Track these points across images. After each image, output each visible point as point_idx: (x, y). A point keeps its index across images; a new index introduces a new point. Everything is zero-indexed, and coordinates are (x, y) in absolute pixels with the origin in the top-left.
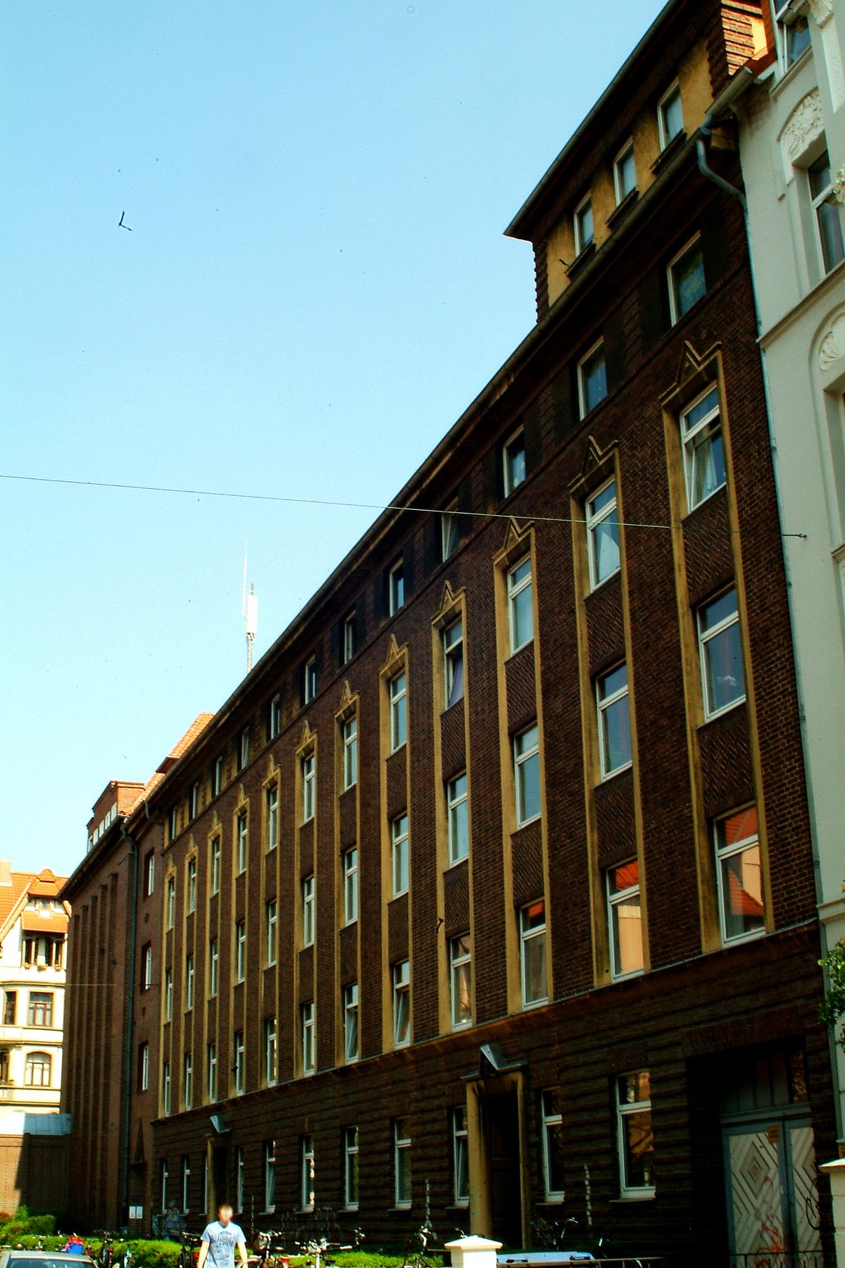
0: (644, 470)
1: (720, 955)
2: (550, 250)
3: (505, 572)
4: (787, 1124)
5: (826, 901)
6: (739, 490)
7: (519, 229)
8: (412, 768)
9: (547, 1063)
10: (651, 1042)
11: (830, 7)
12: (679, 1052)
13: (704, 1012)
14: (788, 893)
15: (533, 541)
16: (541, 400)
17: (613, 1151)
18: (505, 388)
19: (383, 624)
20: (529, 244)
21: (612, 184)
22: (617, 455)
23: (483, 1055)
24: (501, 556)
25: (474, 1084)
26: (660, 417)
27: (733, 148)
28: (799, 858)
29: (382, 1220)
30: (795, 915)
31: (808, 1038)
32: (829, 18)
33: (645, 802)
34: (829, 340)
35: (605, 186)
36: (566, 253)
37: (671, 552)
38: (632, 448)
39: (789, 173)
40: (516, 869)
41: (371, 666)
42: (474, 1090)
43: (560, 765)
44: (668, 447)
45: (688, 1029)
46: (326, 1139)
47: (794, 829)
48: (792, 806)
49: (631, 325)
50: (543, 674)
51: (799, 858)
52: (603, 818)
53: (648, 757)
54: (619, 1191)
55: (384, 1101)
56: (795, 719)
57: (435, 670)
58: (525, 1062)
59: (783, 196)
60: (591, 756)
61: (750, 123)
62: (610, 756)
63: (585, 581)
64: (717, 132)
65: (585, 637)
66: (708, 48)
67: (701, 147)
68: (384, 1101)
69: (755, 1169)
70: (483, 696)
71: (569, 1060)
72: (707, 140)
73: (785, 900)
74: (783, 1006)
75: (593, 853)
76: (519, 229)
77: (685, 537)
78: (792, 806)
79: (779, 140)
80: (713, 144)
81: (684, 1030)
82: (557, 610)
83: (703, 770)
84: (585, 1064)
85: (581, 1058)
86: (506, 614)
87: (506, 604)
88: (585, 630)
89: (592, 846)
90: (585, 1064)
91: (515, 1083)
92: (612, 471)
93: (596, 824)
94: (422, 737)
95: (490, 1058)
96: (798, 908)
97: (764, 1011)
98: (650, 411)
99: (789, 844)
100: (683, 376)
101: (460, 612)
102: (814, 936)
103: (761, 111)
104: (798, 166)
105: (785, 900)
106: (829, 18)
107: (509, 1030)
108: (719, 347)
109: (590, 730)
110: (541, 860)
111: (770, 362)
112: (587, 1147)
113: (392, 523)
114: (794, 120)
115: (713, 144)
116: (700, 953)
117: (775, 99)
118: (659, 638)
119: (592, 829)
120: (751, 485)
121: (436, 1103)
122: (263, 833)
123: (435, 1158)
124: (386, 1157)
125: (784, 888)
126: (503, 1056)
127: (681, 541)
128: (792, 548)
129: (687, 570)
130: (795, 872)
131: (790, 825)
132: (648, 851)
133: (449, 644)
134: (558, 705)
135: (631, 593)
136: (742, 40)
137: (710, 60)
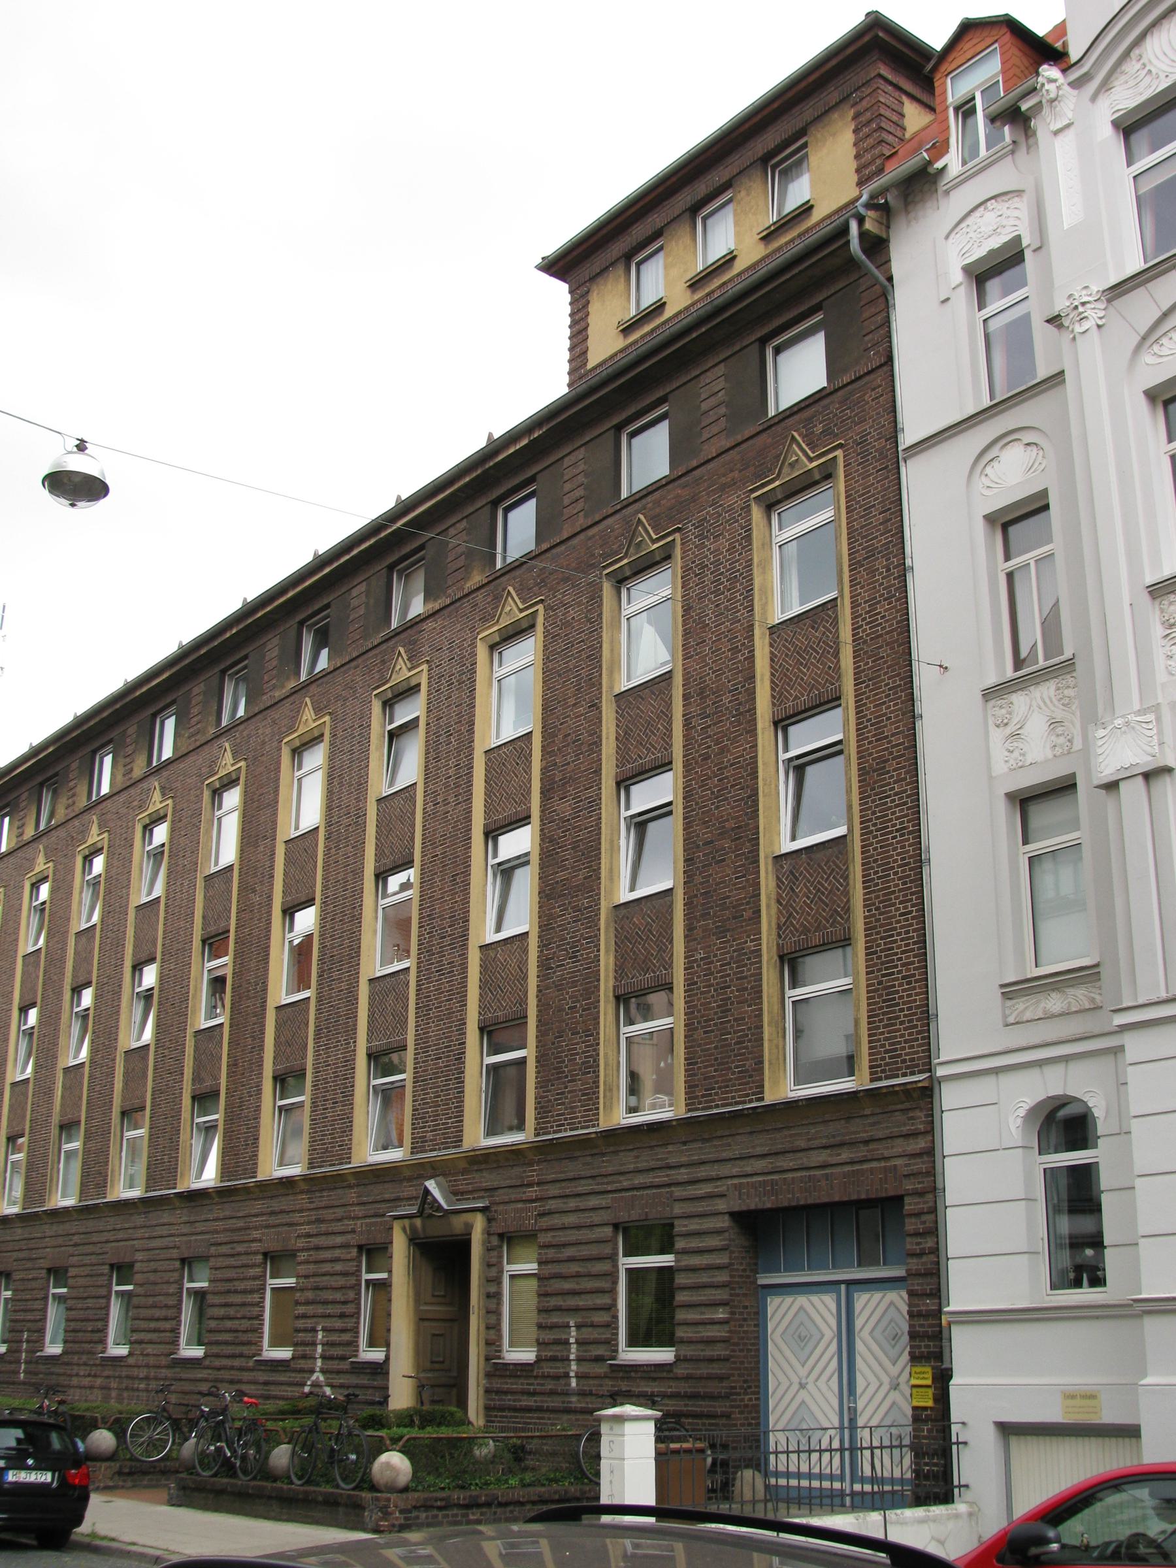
0: (717, 563)
1: (792, 1106)
2: (594, 297)
3: (492, 648)
4: (852, 1287)
5: (942, 1059)
6: (855, 605)
7: (560, 265)
8: (327, 853)
9: (520, 1205)
10: (678, 1192)
11: (1070, 115)
12: (721, 1205)
13: (760, 1165)
14: (890, 1045)
15: (540, 620)
16: (567, 462)
17: (611, 1308)
18: (525, 442)
19: (292, 684)
20: (564, 287)
21: (694, 240)
22: (678, 542)
23: (427, 1192)
24: (491, 631)
25: (407, 1222)
26: (747, 509)
27: (884, 236)
28: (909, 1009)
29: (241, 1369)
30: (898, 1069)
31: (907, 1200)
32: (1068, 126)
33: (689, 928)
34: (995, 463)
35: (687, 240)
36: (613, 308)
37: (751, 658)
38: (701, 536)
39: (958, 276)
40: (484, 985)
41: (268, 731)
42: (404, 1229)
43: (562, 875)
44: (756, 544)
45: (735, 1181)
46: (155, 1271)
47: (904, 978)
48: (903, 952)
49: (712, 401)
50: (544, 771)
51: (909, 1009)
52: (622, 942)
53: (698, 879)
54: (616, 1351)
55: (256, 1234)
56: (915, 864)
57: (372, 747)
58: (487, 1203)
59: (948, 299)
60: (611, 870)
61: (907, 212)
62: (642, 873)
63: (616, 675)
64: (871, 214)
65: (613, 737)
66: (854, 119)
67: (854, 226)
68: (256, 1234)
69: (802, 1338)
70: (447, 786)
71: (552, 1205)
72: (861, 220)
73: (886, 1052)
74: (874, 1164)
75: (607, 976)
76: (560, 265)
77: (771, 645)
78: (903, 952)
79: (947, 237)
80: (868, 225)
81: (730, 1182)
82: (571, 701)
83: (778, 902)
84: (577, 1210)
85: (572, 1204)
86: (489, 695)
87: (490, 685)
88: (613, 729)
89: (606, 970)
90: (577, 1210)
91: (469, 1228)
92: (668, 557)
93: (613, 947)
94: (346, 821)
95: (436, 1193)
96: (904, 1061)
97: (847, 1168)
98: (733, 499)
99: (897, 992)
100: (786, 470)
101: (419, 685)
102: (924, 1097)
103: (923, 200)
104: (967, 270)
105: (886, 1052)
106: (1068, 126)
107: (463, 1165)
108: (840, 446)
109: (612, 841)
110: (525, 978)
111: (916, 478)
112: (580, 1302)
113: (327, 570)
114: (969, 221)
115: (868, 225)
116: (762, 1099)
117: (947, 192)
118: (723, 750)
119: (607, 951)
120: (873, 603)
121: (339, 1240)
122: (74, 906)
123: (334, 1302)
124: (256, 1297)
125: (886, 1039)
126: (455, 1193)
127: (767, 649)
128: (925, 679)
129: (772, 682)
130: (902, 1023)
131: (899, 972)
132: (690, 984)
133: (391, 722)
134: (564, 808)
135: (686, 697)
136: (895, 118)
137: (855, 131)
